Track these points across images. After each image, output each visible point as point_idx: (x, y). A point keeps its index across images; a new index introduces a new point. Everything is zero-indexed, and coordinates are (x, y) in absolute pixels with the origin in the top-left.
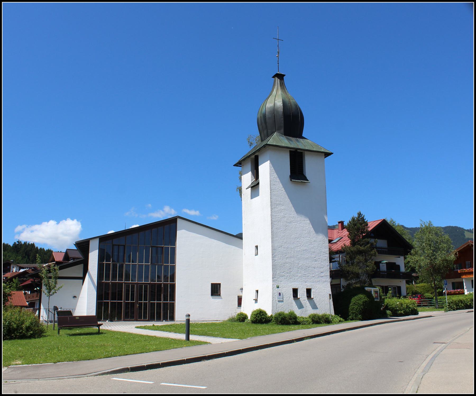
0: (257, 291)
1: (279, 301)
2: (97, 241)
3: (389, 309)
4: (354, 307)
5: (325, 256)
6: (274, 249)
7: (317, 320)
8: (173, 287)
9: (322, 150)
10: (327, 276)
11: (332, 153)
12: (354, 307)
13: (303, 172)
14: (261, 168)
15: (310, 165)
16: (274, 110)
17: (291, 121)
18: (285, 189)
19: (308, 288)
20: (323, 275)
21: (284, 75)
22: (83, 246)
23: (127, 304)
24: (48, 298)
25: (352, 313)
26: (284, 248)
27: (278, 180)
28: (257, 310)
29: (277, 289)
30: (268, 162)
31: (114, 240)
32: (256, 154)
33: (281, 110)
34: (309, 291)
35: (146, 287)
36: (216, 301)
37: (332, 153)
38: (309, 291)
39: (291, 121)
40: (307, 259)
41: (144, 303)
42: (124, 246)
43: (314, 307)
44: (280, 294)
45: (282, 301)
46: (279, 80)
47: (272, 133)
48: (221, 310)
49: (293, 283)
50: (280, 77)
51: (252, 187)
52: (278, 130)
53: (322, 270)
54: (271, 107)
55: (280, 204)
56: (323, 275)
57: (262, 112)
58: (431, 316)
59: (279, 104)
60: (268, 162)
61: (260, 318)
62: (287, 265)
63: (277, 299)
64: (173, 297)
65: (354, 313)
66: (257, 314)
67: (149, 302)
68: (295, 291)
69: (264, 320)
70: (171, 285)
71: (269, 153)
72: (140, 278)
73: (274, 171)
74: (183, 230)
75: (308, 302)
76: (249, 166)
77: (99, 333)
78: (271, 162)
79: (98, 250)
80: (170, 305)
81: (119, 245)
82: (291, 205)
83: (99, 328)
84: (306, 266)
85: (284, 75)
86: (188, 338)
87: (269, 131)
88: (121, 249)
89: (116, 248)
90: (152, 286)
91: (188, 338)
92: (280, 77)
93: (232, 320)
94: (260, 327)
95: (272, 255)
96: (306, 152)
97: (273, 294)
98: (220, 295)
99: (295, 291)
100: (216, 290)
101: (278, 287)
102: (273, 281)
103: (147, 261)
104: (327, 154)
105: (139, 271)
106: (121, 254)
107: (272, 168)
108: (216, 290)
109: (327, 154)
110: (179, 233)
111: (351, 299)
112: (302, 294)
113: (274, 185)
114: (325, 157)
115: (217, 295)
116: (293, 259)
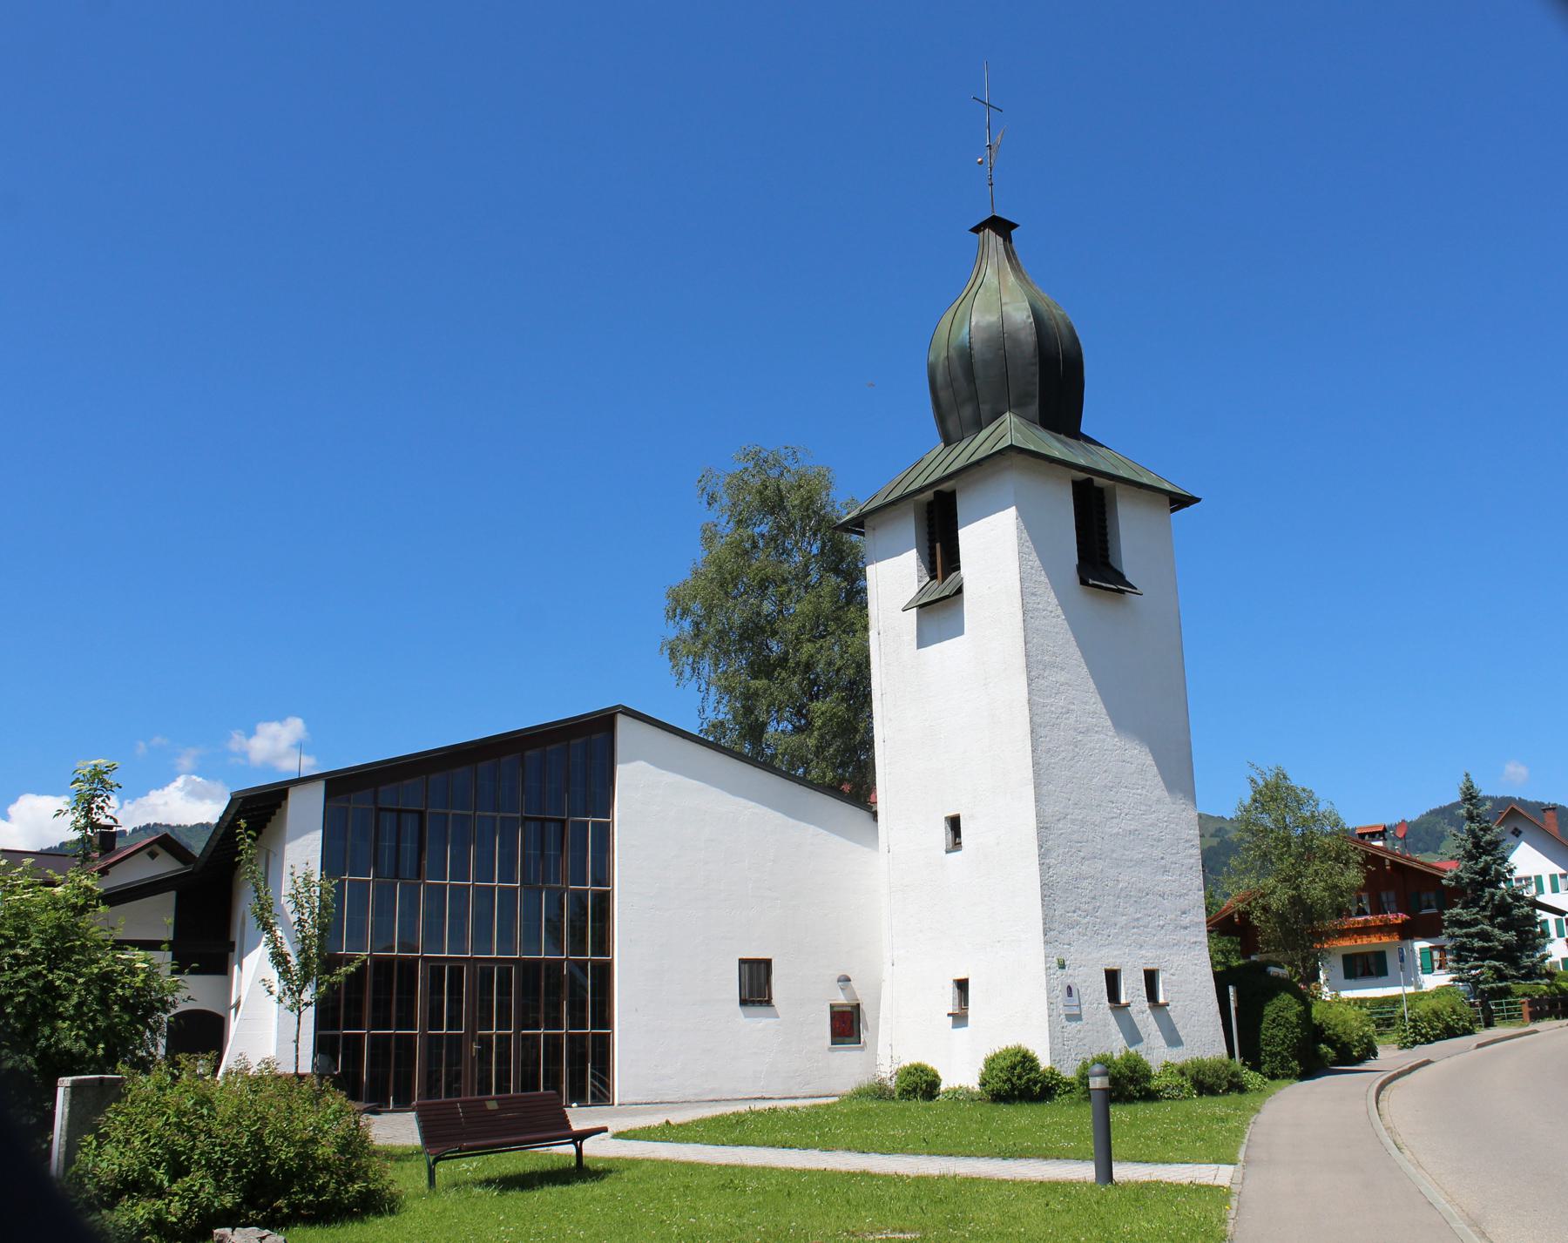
0: (962, 985)
1: (1070, 1018)
2: (319, 790)
3: (1330, 1042)
4: (1275, 1031)
5: (1191, 856)
6: (1043, 828)
7: (1205, 1083)
8: (604, 974)
9: (1167, 487)
10: (1198, 924)
11: (1198, 500)
12: (1275, 1031)
13: (1107, 557)
14: (970, 537)
15: (1135, 534)
16: (1001, 339)
17: (1051, 379)
18: (1065, 612)
19: (1149, 967)
20: (1186, 920)
21: (1014, 226)
22: (259, 810)
23: (433, 1043)
24: (294, 1017)
25: (1272, 1055)
26: (1073, 821)
27: (1044, 579)
28: (1007, 1054)
29: (1059, 972)
30: (1012, 511)
31: (381, 789)
32: (945, 487)
33: (1028, 337)
34: (1151, 978)
35: (456, 974)
36: (756, 1023)
37: (1198, 500)
38: (1151, 978)
39: (1051, 379)
40: (1141, 862)
41: (499, 1036)
42: (421, 814)
43: (1173, 1039)
44: (1069, 988)
45: (1078, 1018)
46: (1000, 240)
47: (997, 415)
48: (782, 1059)
49: (1105, 951)
50: (1002, 227)
51: (921, 607)
52: (1018, 406)
53: (1183, 903)
54: (989, 326)
55: (1053, 665)
56: (1186, 920)
57: (954, 343)
58: (1428, 1062)
59: (1019, 314)
60: (1012, 511)
61: (1018, 1083)
62: (1085, 884)
63: (1062, 1011)
64: (603, 1017)
65: (1276, 1054)
66: (1013, 1067)
67: (517, 1032)
68: (1112, 978)
69: (1037, 1089)
70: (595, 965)
71: (1011, 480)
72: (458, 940)
73: (1029, 544)
74: (643, 763)
75: (1151, 1018)
76: (907, 527)
77: (580, 1171)
78: (1022, 514)
79: (320, 833)
80: (398, 1047)
81: (399, 811)
82: (1084, 670)
83: (579, 1151)
84: (1140, 890)
85: (1014, 226)
86: (1105, 1174)
87: (985, 409)
88: (410, 824)
89: (388, 821)
90: (530, 970)
91: (1105, 1174)
92: (1002, 227)
93: (860, 1094)
94: (1021, 1116)
95: (1040, 847)
96: (1120, 489)
97: (1050, 990)
98: (768, 1003)
99: (1112, 978)
100: (756, 983)
101: (1062, 966)
102: (1046, 942)
103: (507, 875)
104: (1179, 501)
105: (469, 918)
106: (409, 846)
107: (1025, 535)
108: (756, 983)
109: (1179, 501)
110: (623, 773)
111: (1262, 1009)
112: (1132, 989)
113: (1034, 594)
114: (1173, 511)
115: (761, 1003)
116: (1099, 865)
